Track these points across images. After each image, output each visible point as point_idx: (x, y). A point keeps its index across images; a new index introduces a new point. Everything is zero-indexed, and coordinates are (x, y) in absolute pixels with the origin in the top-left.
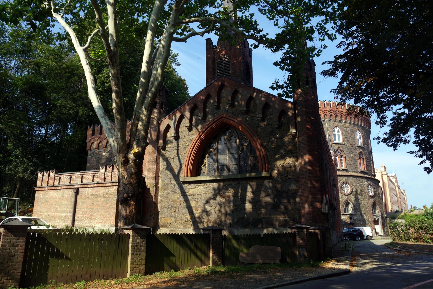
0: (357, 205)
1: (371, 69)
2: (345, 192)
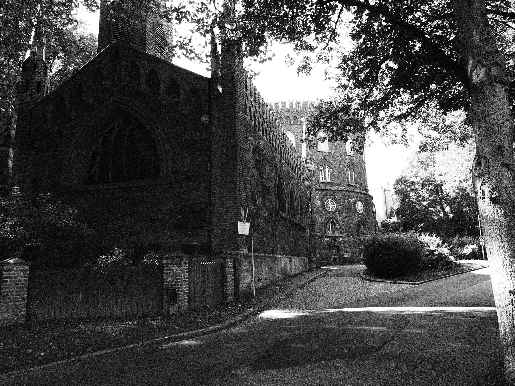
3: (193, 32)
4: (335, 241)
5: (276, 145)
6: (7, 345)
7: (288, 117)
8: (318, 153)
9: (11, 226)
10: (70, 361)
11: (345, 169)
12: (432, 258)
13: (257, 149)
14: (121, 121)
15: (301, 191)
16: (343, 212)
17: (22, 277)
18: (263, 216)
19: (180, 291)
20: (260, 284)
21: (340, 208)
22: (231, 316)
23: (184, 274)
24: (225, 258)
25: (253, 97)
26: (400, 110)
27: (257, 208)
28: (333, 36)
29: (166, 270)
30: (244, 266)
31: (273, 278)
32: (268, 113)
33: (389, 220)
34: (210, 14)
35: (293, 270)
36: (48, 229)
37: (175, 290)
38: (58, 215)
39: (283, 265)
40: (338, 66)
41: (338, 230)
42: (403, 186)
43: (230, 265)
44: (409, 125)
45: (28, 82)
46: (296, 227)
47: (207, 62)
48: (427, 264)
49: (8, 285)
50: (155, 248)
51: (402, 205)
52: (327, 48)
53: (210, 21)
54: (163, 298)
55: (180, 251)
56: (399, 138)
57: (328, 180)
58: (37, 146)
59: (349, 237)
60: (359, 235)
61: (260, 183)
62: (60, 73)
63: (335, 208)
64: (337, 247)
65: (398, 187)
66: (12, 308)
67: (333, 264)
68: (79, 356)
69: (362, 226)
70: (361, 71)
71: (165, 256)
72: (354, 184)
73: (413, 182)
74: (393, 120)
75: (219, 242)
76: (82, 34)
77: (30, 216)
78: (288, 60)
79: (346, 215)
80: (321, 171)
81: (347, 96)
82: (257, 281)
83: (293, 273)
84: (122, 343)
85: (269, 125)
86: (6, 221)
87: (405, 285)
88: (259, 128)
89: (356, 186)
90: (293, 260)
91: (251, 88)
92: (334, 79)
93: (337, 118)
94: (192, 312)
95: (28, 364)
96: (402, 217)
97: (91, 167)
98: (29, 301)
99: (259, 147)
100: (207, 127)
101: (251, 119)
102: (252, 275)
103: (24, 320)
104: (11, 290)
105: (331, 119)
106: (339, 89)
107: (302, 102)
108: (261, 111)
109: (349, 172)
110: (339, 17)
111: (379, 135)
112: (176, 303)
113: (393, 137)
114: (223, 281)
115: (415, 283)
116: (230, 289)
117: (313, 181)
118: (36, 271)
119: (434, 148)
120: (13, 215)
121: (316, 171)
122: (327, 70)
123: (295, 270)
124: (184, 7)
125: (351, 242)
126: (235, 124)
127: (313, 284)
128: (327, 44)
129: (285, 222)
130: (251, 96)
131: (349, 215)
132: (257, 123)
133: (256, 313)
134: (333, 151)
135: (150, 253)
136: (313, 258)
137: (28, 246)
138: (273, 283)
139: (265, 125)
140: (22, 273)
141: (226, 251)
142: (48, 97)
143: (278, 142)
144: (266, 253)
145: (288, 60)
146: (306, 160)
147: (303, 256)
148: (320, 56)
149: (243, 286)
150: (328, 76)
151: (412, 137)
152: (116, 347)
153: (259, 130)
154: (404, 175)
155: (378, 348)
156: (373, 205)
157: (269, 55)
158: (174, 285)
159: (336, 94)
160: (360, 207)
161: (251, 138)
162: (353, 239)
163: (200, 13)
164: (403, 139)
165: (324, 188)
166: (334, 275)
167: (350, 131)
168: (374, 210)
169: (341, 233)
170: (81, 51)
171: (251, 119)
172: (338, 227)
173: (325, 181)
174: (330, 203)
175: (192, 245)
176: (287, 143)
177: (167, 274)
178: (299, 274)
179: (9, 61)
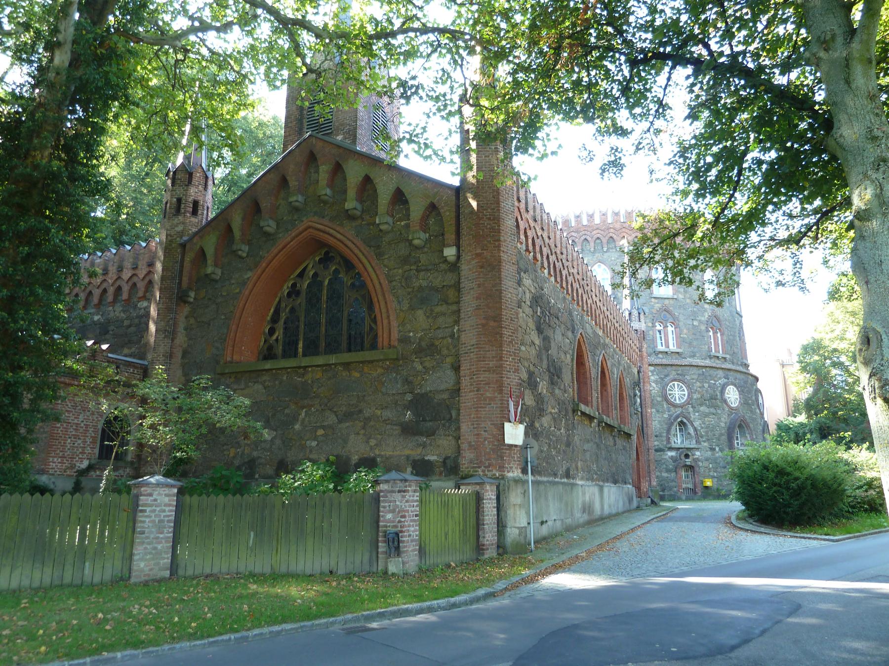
3: (429, 117)
4: (687, 456)
5: (572, 291)
6: (143, 608)
7: (598, 238)
8: (653, 300)
9: (153, 427)
10: (233, 637)
11: (703, 328)
12: (869, 493)
13: (537, 300)
14: (317, 259)
15: (621, 368)
16: (701, 405)
17: (166, 505)
18: (551, 413)
19: (406, 536)
20: (544, 530)
21: (695, 397)
22: (489, 581)
23: (413, 509)
24: (481, 484)
25: (531, 212)
26: (788, 228)
27: (539, 399)
28: (661, 110)
29: (383, 501)
30: (514, 498)
31: (569, 521)
32: (558, 237)
33: (791, 419)
34: (456, 85)
35: (606, 507)
36: (204, 430)
37: (397, 534)
38: (219, 408)
39: (587, 499)
40: (668, 162)
41: (692, 437)
42: (816, 358)
43: (490, 494)
44: (805, 254)
45: (179, 201)
46: (612, 431)
47: (452, 161)
48: (859, 503)
49: (147, 516)
50: (370, 463)
51: (816, 392)
52: (652, 130)
53: (456, 98)
54: (377, 547)
55: (409, 469)
56: (788, 277)
57: (673, 347)
58: (192, 300)
59: (712, 449)
60: (731, 447)
61: (544, 357)
62: (230, 181)
63: (686, 398)
64: (691, 468)
65: (808, 359)
66: (150, 553)
67: (684, 498)
68: (247, 630)
69: (737, 430)
70: (709, 167)
71: (382, 478)
72: (720, 354)
73: (835, 350)
74: (775, 246)
75: (472, 456)
76: (262, 117)
77: (179, 410)
78: (585, 153)
79: (707, 410)
80: (660, 331)
81: (689, 208)
82: (539, 525)
83: (607, 511)
84: (308, 616)
85: (560, 257)
86: (144, 417)
87: (811, 541)
88: (542, 263)
89: (725, 358)
90: (606, 490)
91: (526, 198)
92: (666, 181)
93: (674, 247)
94: (424, 572)
95: (174, 638)
96: (816, 414)
97: (272, 331)
98: (176, 541)
99: (541, 297)
100: (454, 267)
101: (527, 250)
102: (528, 513)
103: (168, 572)
104: (150, 525)
105: (662, 248)
106: (675, 197)
107: (622, 213)
108: (545, 235)
109: (711, 334)
110: (669, 79)
111: (751, 272)
112: (399, 555)
113: (776, 275)
114: (479, 524)
115: (832, 537)
116: (489, 536)
117: (644, 350)
118: (187, 498)
119: (854, 294)
120: (155, 409)
121: (651, 333)
122: (653, 167)
123: (610, 506)
124: (414, 78)
125: (716, 459)
126: (500, 261)
127: (640, 533)
128: (652, 123)
129: (591, 423)
130: (527, 211)
131: (712, 410)
132: (539, 256)
133: (532, 579)
134: (681, 296)
135: (360, 472)
136: (645, 486)
137: (175, 457)
138: (569, 529)
139: (552, 258)
140: (166, 499)
141: (484, 471)
142: (209, 223)
143: (576, 285)
144: (555, 475)
145: (585, 153)
146: (630, 314)
147: (625, 483)
148: (640, 143)
149: (512, 533)
150: (654, 176)
151: (812, 275)
152: (303, 621)
153: (543, 267)
154: (818, 336)
155: (733, 648)
156: (758, 391)
157: (551, 146)
158: (396, 526)
159: (668, 207)
160: (733, 395)
161: (527, 282)
162: (720, 454)
163: (440, 85)
164: (795, 279)
165: (665, 361)
166: (682, 519)
167: (696, 267)
168: (760, 401)
169: (698, 442)
170: (259, 143)
171: (527, 250)
172: (691, 431)
173: (667, 350)
174: (676, 389)
175: (429, 461)
176: (593, 286)
177: (384, 507)
178: (617, 515)
179: (152, 167)
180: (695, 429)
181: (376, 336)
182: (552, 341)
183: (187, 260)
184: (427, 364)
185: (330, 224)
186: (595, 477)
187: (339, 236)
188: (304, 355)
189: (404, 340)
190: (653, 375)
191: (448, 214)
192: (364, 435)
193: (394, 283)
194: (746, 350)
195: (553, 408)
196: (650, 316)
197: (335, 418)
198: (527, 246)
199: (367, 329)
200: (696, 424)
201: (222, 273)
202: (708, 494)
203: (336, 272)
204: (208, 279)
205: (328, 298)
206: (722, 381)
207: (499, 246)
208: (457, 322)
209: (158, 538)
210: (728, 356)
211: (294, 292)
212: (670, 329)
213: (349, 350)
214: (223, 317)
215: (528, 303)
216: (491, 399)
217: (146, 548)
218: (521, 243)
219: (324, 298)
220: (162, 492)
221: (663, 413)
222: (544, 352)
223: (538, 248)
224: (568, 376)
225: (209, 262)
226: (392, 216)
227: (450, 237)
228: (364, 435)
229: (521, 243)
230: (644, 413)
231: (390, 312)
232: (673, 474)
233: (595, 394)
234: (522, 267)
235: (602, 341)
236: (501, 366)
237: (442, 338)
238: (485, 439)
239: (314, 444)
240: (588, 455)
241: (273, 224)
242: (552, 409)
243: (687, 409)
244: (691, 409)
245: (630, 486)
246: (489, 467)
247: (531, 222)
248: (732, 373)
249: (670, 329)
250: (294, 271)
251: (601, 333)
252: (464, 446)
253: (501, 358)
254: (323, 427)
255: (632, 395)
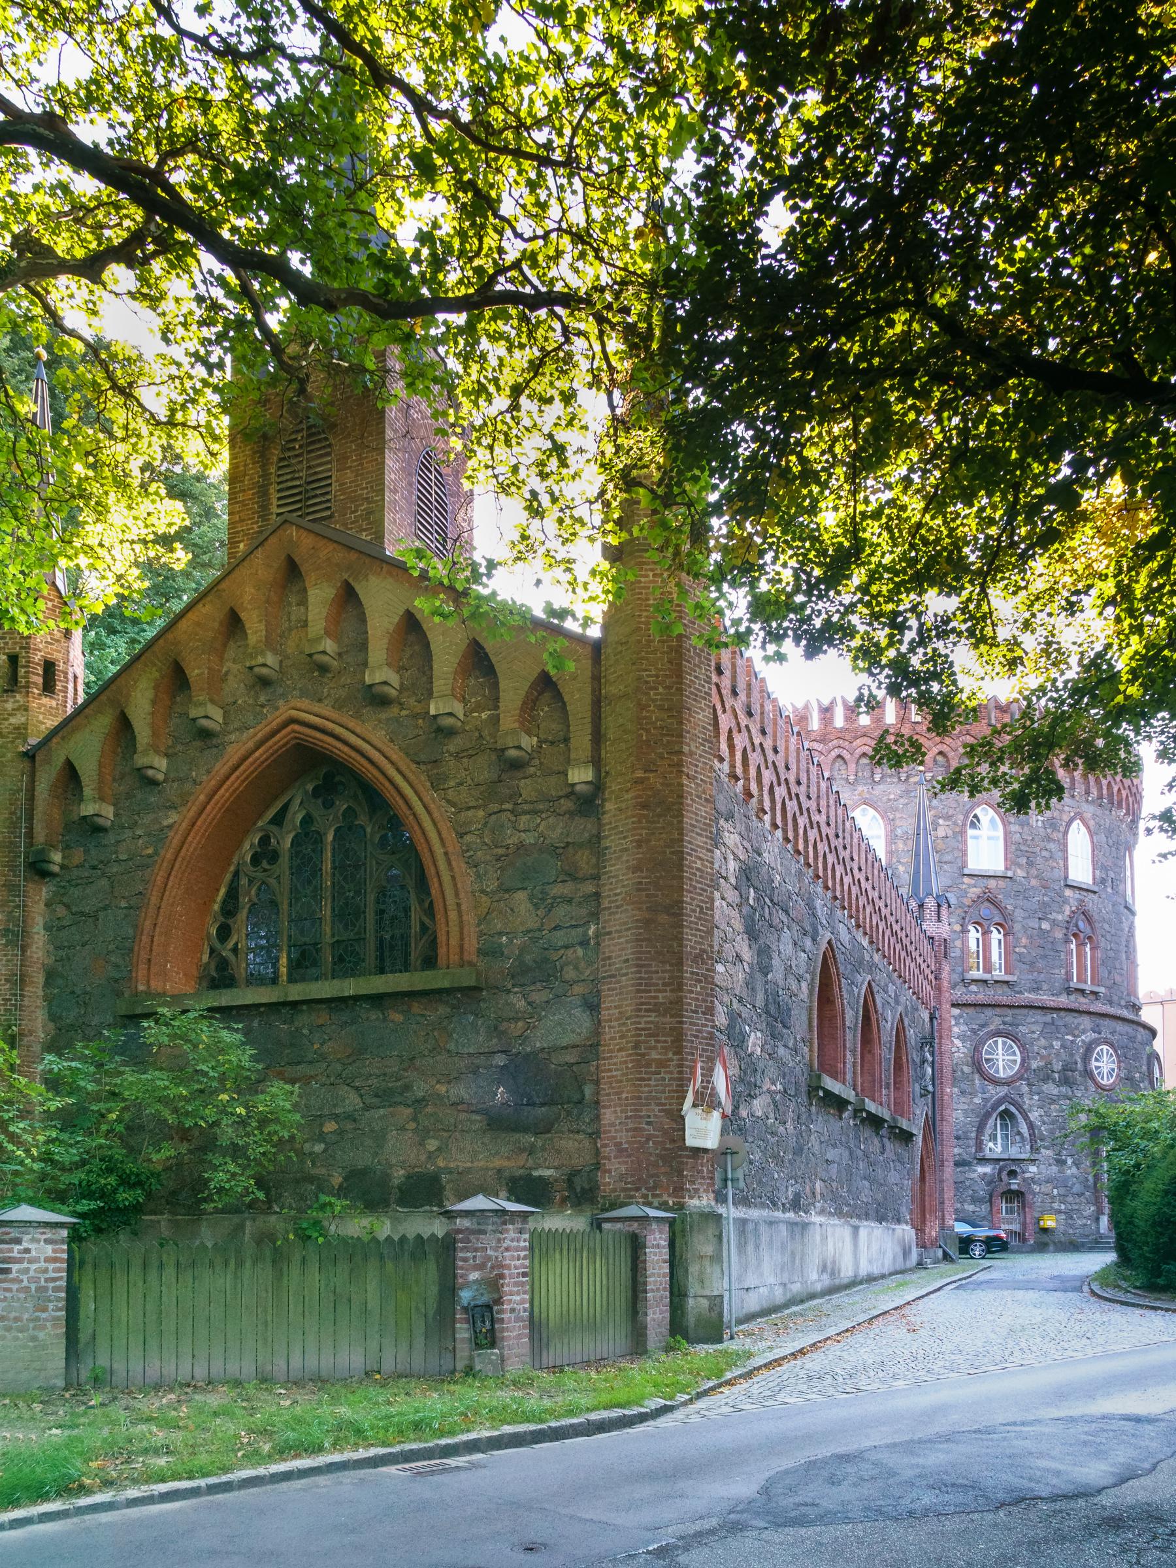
0: (1044, 1123)
1: (870, 364)
2: (997, 1071)
4: (1012, 1174)
8: (966, 880)
11: (1059, 934)
14: (310, 787)
17: (47, 1260)
18: (769, 1091)
25: (742, 696)
29: (463, 1249)
32: (792, 748)
49: (13, 1281)
59: (1061, 1162)
61: (759, 986)
72: (1088, 987)
88: (761, 802)
89: (1095, 993)
90: (863, 1233)
91: (734, 665)
99: (757, 866)
108: (768, 744)
109: (1073, 946)
117: (945, 974)
121: (958, 943)
125: (1067, 1179)
130: (735, 693)
140: (49, 1249)
143: (822, 847)
147: (899, 1221)
160: (1105, 1064)
165: (981, 998)
169: (1034, 1149)
171: (734, 777)
173: (987, 976)
177: (465, 1260)
180: (1031, 1126)
181: (433, 943)
182: (775, 955)
183: (42, 787)
184: (537, 997)
185: (334, 715)
186: (845, 1209)
187: (353, 739)
188: (291, 980)
189: (490, 952)
190: (957, 1024)
191: (578, 699)
192: (415, 1130)
193: (468, 838)
194: (1135, 978)
195: (774, 1083)
196: (959, 911)
197: (358, 1100)
198: (733, 766)
199: (415, 928)
200: (1034, 1116)
201: (116, 815)
202: (1045, 1242)
203: (350, 813)
204: (92, 828)
205: (334, 868)
206: (1089, 1036)
207: (680, 764)
208: (595, 916)
209: (37, 1319)
210: (1102, 990)
211: (265, 854)
212: (996, 936)
213: (382, 971)
214: (123, 904)
215: (733, 881)
216: (662, 1064)
217: (16, 1339)
218: (722, 760)
219: (327, 866)
220: (37, 1236)
221: (973, 1094)
222: (759, 976)
223: (753, 772)
224: (801, 1020)
225: (88, 791)
226: (464, 700)
227: (581, 741)
228: (415, 1130)
229: (722, 760)
230: (938, 1095)
231: (462, 895)
232: (985, 1208)
233: (849, 1058)
234: (723, 809)
235: (867, 958)
236: (679, 1001)
237: (566, 947)
238: (648, 1138)
239: (319, 1148)
240: (834, 1168)
241: (217, 714)
242: (771, 1084)
243: (1019, 1087)
244: (1025, 1089)
245: (907, 1228)
246: (655, 1188)
247: (742, 716)
248: (1107, 1022)
249: (996, 936)
250: (268, 807)
251: (865, 943)
252: (609, 1150)
253: (680, 987)
254: (335, 1117)
255: (917, 1060)
